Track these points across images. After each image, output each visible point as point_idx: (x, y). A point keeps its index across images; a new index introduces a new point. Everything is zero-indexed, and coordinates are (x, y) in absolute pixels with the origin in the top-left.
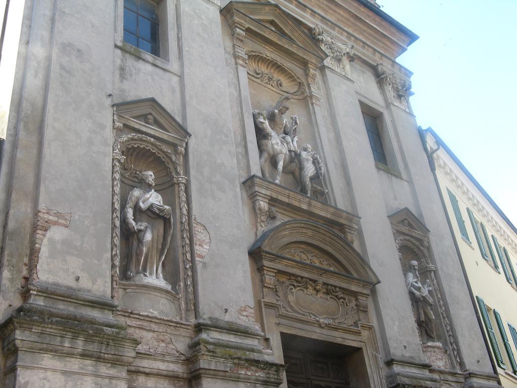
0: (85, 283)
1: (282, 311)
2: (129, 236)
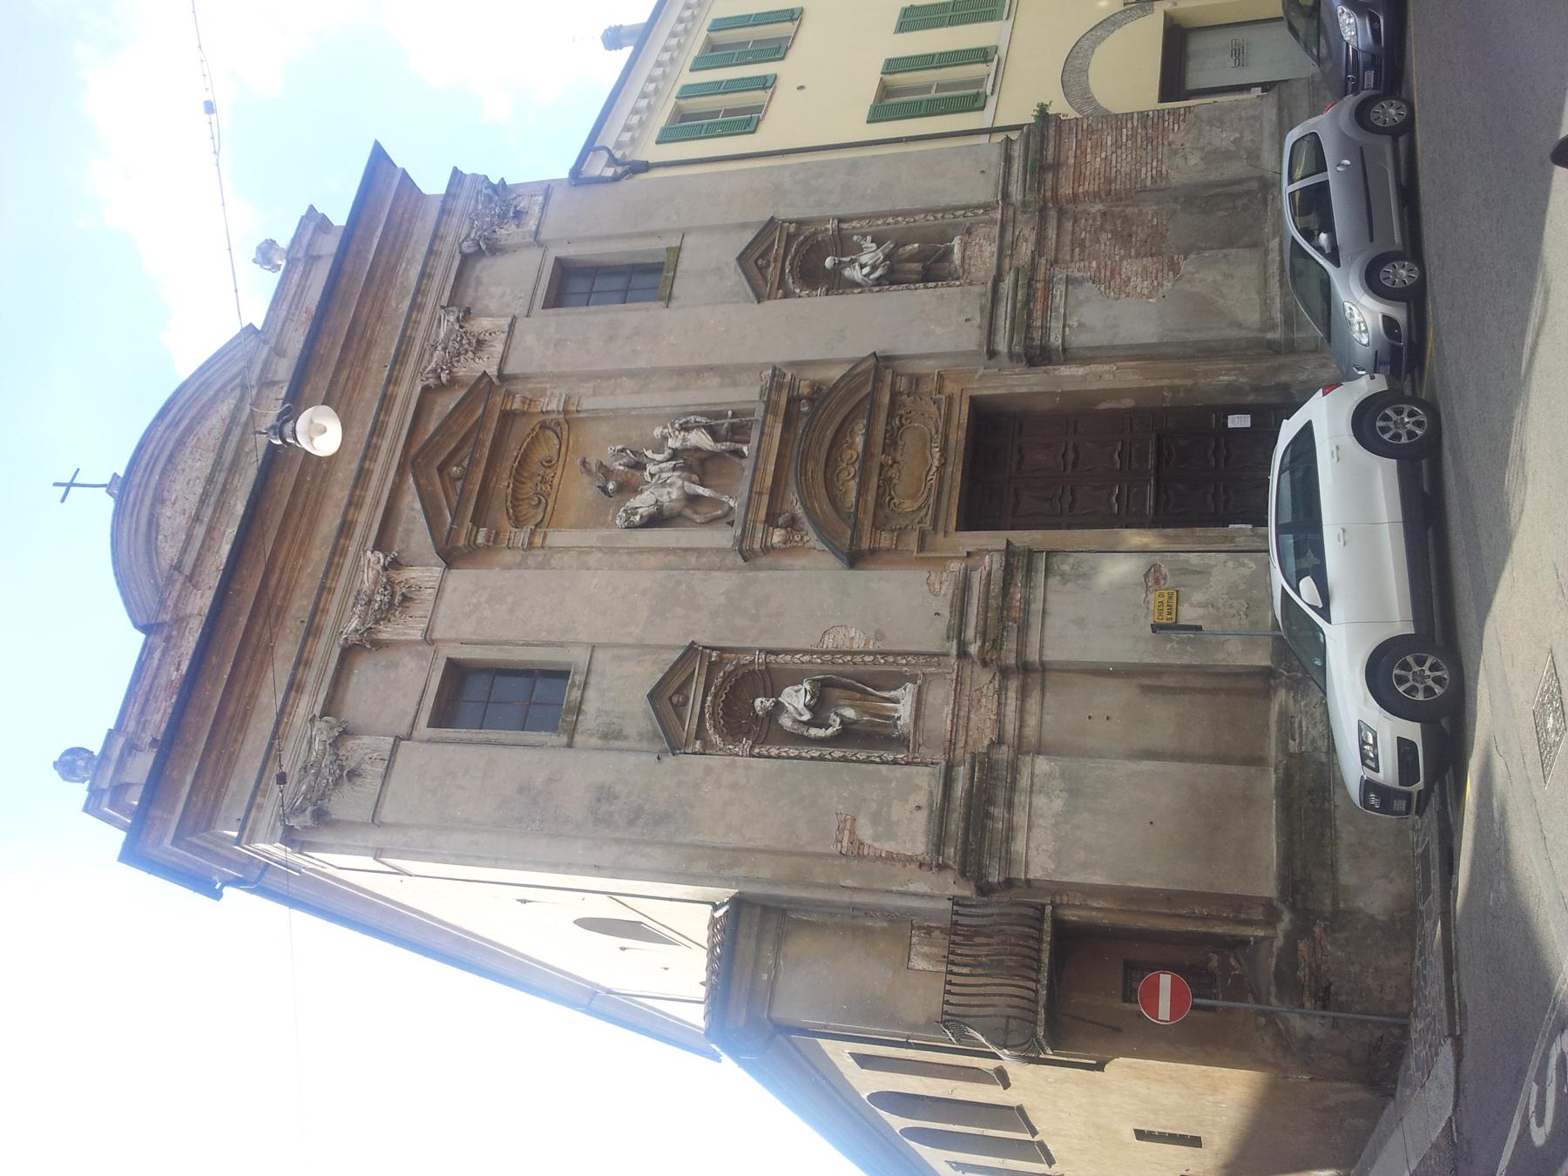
0: (921, 798)
1: (927, 525)
2: (848, 735)
